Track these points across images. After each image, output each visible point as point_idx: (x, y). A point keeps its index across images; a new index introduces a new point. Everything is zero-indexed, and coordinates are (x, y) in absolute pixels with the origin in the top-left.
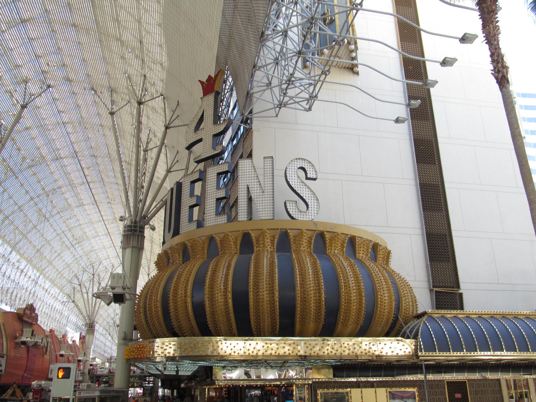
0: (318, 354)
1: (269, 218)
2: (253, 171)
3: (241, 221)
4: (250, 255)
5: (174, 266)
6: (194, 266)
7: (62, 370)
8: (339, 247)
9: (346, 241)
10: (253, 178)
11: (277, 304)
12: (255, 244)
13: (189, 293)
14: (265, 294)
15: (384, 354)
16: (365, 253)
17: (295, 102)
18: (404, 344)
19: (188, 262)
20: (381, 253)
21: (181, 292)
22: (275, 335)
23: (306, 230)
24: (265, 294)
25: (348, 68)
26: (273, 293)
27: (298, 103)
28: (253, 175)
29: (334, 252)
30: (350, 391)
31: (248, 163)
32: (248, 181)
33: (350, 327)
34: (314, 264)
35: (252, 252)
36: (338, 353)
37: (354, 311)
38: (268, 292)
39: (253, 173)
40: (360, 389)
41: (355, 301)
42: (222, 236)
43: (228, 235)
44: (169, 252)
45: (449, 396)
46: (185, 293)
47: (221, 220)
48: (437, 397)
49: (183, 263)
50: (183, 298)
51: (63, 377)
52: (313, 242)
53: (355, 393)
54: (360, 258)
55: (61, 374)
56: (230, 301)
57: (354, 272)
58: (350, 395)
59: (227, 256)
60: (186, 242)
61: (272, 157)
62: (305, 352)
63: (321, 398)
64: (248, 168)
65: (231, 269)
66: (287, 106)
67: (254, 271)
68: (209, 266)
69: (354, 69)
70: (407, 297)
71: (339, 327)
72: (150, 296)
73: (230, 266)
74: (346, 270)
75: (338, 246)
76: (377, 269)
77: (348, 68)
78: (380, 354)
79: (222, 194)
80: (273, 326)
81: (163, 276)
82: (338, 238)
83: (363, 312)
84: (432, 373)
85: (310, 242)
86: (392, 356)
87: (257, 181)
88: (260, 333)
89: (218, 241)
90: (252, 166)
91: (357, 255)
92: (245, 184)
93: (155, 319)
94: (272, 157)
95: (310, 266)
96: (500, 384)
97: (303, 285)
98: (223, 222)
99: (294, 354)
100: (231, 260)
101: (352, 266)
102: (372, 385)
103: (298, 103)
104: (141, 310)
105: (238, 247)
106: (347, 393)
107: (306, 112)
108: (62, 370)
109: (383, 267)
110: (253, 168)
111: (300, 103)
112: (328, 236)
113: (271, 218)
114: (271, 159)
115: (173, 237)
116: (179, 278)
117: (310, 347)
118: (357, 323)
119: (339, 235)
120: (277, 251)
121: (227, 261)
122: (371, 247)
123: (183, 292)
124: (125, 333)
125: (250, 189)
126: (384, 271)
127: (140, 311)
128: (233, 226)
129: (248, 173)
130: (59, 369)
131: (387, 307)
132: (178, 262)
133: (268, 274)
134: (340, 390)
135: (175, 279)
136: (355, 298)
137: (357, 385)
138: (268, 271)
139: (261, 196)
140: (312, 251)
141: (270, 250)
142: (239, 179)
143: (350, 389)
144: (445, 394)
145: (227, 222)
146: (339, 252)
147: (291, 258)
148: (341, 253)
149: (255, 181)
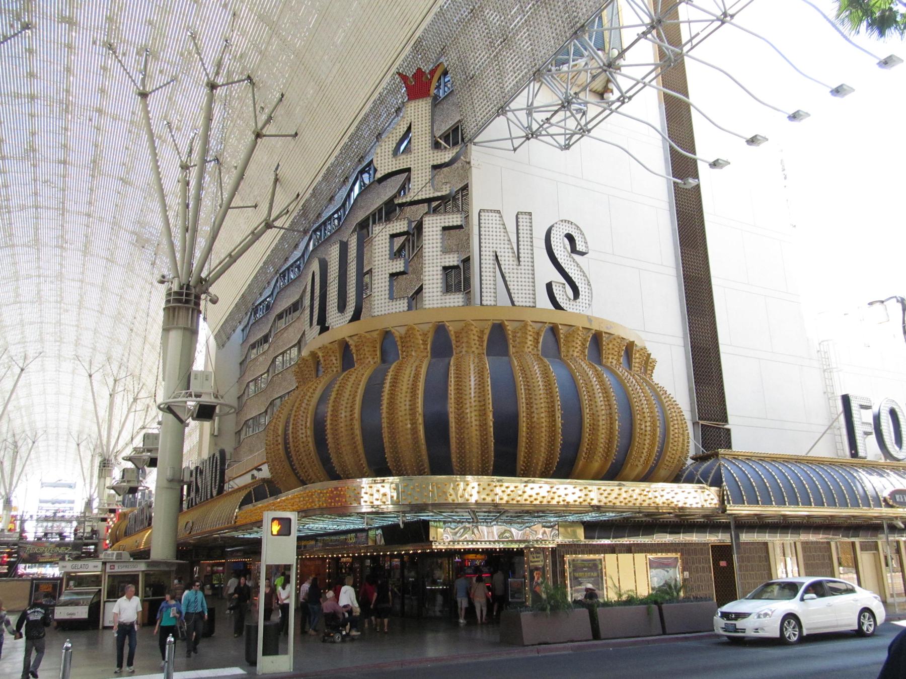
0: (703, 506)
1: (528, 304)
2: (502, 230)
3: (487, 305)
4: (447, 360)
5: (329, 376)
6: (361, 376)
7: (276, 522)
8: (579, 348)
9: (589, 339)
10: (502, 242)
11: (492, 429)
12: (454, 342)
13: (357, 415)
14: (472, 417)
15: (687, 506)
16: (615, 357)
18: (709, 493)
19: (352, 370)
20: (637, 355)
21: (343, 414)
22: (487, 475)
23: (532, 322)
24: (472, 417)
26: (554, 416)
28: (502, 238)
29: (572, 355)
30: (604, 557)
31: (494, 218)
32: (495, 245)
33: (596, 465)
34: (546, 374)
35: (451, 355)
36: (638, 503)
37: (602, 441)
38: (476, 413)
39: (502, 234)
40: (615, 555)
41: (604, 427)
42: (403, 331)
43: (414, 329)
44: (320, 354)
45: (713, 564)
46: (351, 415)
48: (701, 566)
49: (344, 370)
50: (348, 423)
51: (279, 534)
52: (541, 340)
53: (610, 558)
54: (609, 364)
55: (276, 528)
56: (421, 428)
57: (601, 382)
58: (603, 563)
59: (413, 360)
60: (348, 339)
61: (530, 214)
62: (600, 501)
63: (570, 567)
64: (494, 226)
67: (455, 382)
68: (386, 376)
70: (676, 422)
71: (581, 463)
72: (295, 416)
73: (418, 375)
74: (591, 382)
75: (577, 346)
76: (634, 381)
78: (684, 506)
79: (453, 260)
80: (548, 463)
81: (314, 390)
82: (578, 334)
83: (616, 442)
84: (697, 532)
85: (536, 341)
86: (697, 508)
87: (509, 246)
88: (528, 472)
89: (452, 333)
90: (501, 222)
91: (604, 360)
92: (491, 250)
94: (530, 214)
95: (540, 376)
96: (314, 537)
97: (529, 404)
99: (586, 503)
100: (418, 368)
101: (599, 376)
102: (629, 549)
104: (280, 440)
105: (485, 344)
106: (600, 560)
108: (276, 522)
109: (643, 379)
110: (502, 226)
112: (562, 331)
113: (532, 304)
115: (320, 333)
116: (339, 394)
117: (605, 494)
118: (605, 458)
119: (578, 329)
120: (488, 355)
121: (414, 368)
122: (624, 348)
123: (348, 414)
124: (174, 468)
125: (499, 258)
126: (645, 384)
127: (277, 441)
128: (414, 318)
129: (494, 234)
130: (274, 519)
131: (649, 437)
132: (335, 370)
134: (592, 556)
135: (333, 395)
136: (604, 422)
137: (612, 549)
139: (515, 271)
140: (540, 353)
141: (476, 352)
143: (602, 555)
144: (709, 562)
145: (408, 310)
146: (578, 354)
147: (510, 363)
148: (582, 357)
149: (506, 246)
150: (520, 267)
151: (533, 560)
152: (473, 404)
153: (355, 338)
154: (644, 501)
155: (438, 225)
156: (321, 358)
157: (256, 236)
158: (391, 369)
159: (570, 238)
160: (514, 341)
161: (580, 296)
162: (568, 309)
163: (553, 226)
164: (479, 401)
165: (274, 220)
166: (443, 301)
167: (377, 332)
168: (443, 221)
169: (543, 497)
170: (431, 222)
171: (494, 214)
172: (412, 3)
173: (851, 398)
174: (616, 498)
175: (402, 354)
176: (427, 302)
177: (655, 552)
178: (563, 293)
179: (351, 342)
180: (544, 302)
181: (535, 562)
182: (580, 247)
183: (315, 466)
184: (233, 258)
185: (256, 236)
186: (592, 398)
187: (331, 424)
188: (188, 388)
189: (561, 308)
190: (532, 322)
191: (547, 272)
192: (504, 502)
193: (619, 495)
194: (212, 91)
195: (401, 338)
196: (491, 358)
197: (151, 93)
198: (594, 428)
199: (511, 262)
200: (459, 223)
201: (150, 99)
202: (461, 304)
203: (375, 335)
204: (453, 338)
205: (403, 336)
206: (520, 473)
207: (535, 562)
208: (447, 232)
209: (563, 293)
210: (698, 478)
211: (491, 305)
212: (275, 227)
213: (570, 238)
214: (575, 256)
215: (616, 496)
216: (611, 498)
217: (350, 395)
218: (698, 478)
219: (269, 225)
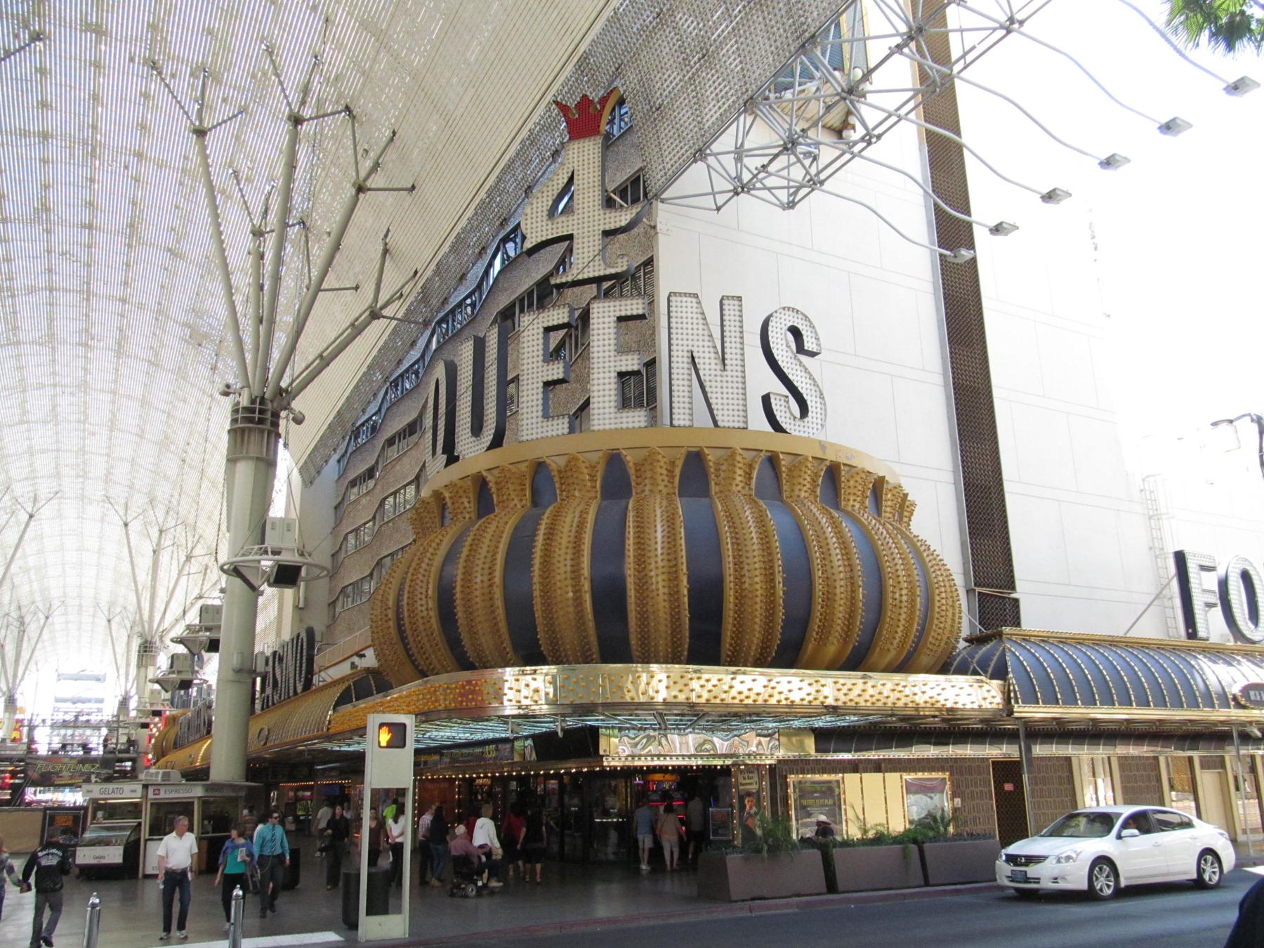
0: (980, 706)
2: (701, 321)
3: (679, 426)
4: (623, 502)
5: (459, 525)
6: (503, 524)
8: (808, 486)
9: (822, 474)
10: (701, 338)
11: (686, 599)
12: (633, 477)
13: (498, 579)
14: (659, 582)
15: (959, 706)
16: (859, 499)
17: (765, 188)
19: (492, 516)
20: (889, 496)
21: (479, 578)
22: (679, 663)
23: (743, 449)
24: (659, 582)
25: (829, 128)
27: (769, 189)
28: (701, 332)
29: (799, 496)
30: (843, 778)
31: (689, 305)
32: (690, 343)
33: (831, 649)
34: (761, 522)
35: (629, 495)
36: (890, 703)
37: (840, 615)
38: (665, 577)
39: (701, 327)
40: (858, 775)
41: (843, 596)
42: (562, 462)
43: (577, 459)
44: (447, 495)
45: (995, 788)
46: (489, 580)
47: (630, 420)
48: (978, 790)
49: (480, 516)
50: (486, 591)
51: (390, 745)
52: (755, 475)
53: (851, 780)
54: (849, 509)
56: (587, 598)
57: (839, 534)
58: (842, 786)
59: (576, 503)
60: (485, 474)
61: (739, 299)
62: (837, 700)
63: (795, 792)
64: (689, 315)
65: (588, 525)
66: (752, 192)
67: (634, 533)
68: (539, 524)
69: (845, 134)
70: (943, 589)
71: (810, 646)
72: (412, 580)
73: (583, 524)
74: (824, 533)
75: (805, 482)
76: (885, 532)
77: (829, 128)
78: (955, 706)
79: (631, 363)
80: (765, 646)
81: (438, 544)
82: (807, 467)
83: (859, 617)
84: (972, 743)
85: (748, 476)
86: (973, 709)
87: (710, 344)
88: (736, 660)
89: (631, 464)
90: (699, 310)
91: (843, 503)
92: (686, 348)
93: (424, 634)
94: (739, 299)
95: (753, 525)
96: (438, 750)
97: (738, 564)
98: (636, 425)
99: (817, 703)
100: (583, 513)
101: (835, 525)
102: (877, 766)
103: (769, 189)
104: (391, 614)
105: (677, 480)
106: (838, 782)
107: (781, 210)
109: (897, 529)
110: (700, 316)
111: (773, 191)
112: (785, 462)
114: (737, 303)
115: (446, 466)
116: (473, 550)
117: (845, 690)
118: (845, 640)
119: (807, 460)
120: (680, 496)
121: (577, 514)
122: (871, 486)
123: (486, 578)
124: (242, 653)
125: (697, 360)
126: (899, 537)
127: (386, 616)
129: (690, 326)
131: (905, 610)
132: (467, 516)
133: (571, 545)
134: (826, 777)
135: (465, 551)
136: (842, 589)
137: (854, 767)
138: (572, 539)
139: (719, 379)
140: (753, 493)
141: (665, 491)
142: (591, 350)
143: (841, 775)
144: (990, 785)
145: (569, 433)
146: (807, 495)
147: (712, 506)
148: (812, 498)
149: (707, 344)
150: (725, 373)
151: (744, 782)
152: (661, 564)
153: (496, 472)
154: (898, 699)
155: (612, 314)
156: (448, 500)
157: (357, 329)
158: (546, 515)
159: (795, 332)
160: (717, 476)
161: (810, 414)
162: (792, 432)
163: (771, 316)
164: (669, 560)
165: (382, 308)
166: (618, 421)
167: (526, 464)
168: (617, 308)
169: (758, 694)
170: (601, 310)
171: (689, 299)
172: (575, 4)
173: (1187, 556)
174: (859, 695)
175: (561, 495)
176: (595, 422)
177: (914, 770)
178: (785, 410)
179: (489, 478)
180: (759, 422)
181: (747, 784)
182: (809, 344)
183: (439, 651)
184: (325, 361)
185: (357, 329)
186: (826, 555)
187: (462, 592)
188: (263, 542)
189: (783, 431)
190: (743, 449)
191: (763, 380)
192: (703, 700)
193: (864, 691)
194: (296, 127)
195: (560, 472)
196: (685, 499)
197: (210, 130)
198: (829, 598)
199: (713, 366)
200: (640, 312)
201: (209, 138)
202: (643, 424)
203: (523, 467)
204: (632, 472)
205: (563, 469)
206: (726, 661)
207: (747, 784)
208: (624, 324)
209: (785, 410)
210: (974, 668)
211: (684, 426)
212: (384, 317)
213: (795, 332)
214: (802, 358)
215: (860, 692)
216: (853, 695)
217: (488, 552)
218: (974, 668)
219: (375, 315)
